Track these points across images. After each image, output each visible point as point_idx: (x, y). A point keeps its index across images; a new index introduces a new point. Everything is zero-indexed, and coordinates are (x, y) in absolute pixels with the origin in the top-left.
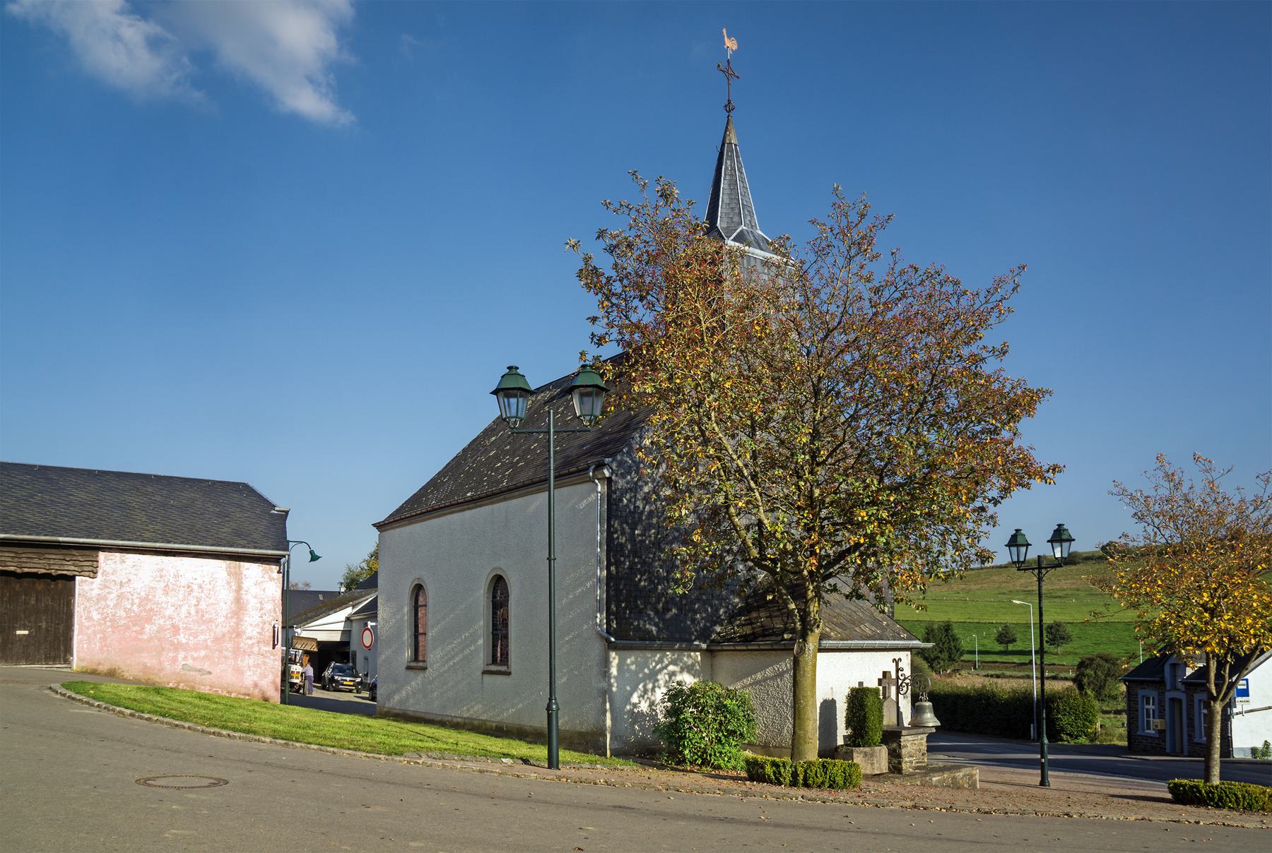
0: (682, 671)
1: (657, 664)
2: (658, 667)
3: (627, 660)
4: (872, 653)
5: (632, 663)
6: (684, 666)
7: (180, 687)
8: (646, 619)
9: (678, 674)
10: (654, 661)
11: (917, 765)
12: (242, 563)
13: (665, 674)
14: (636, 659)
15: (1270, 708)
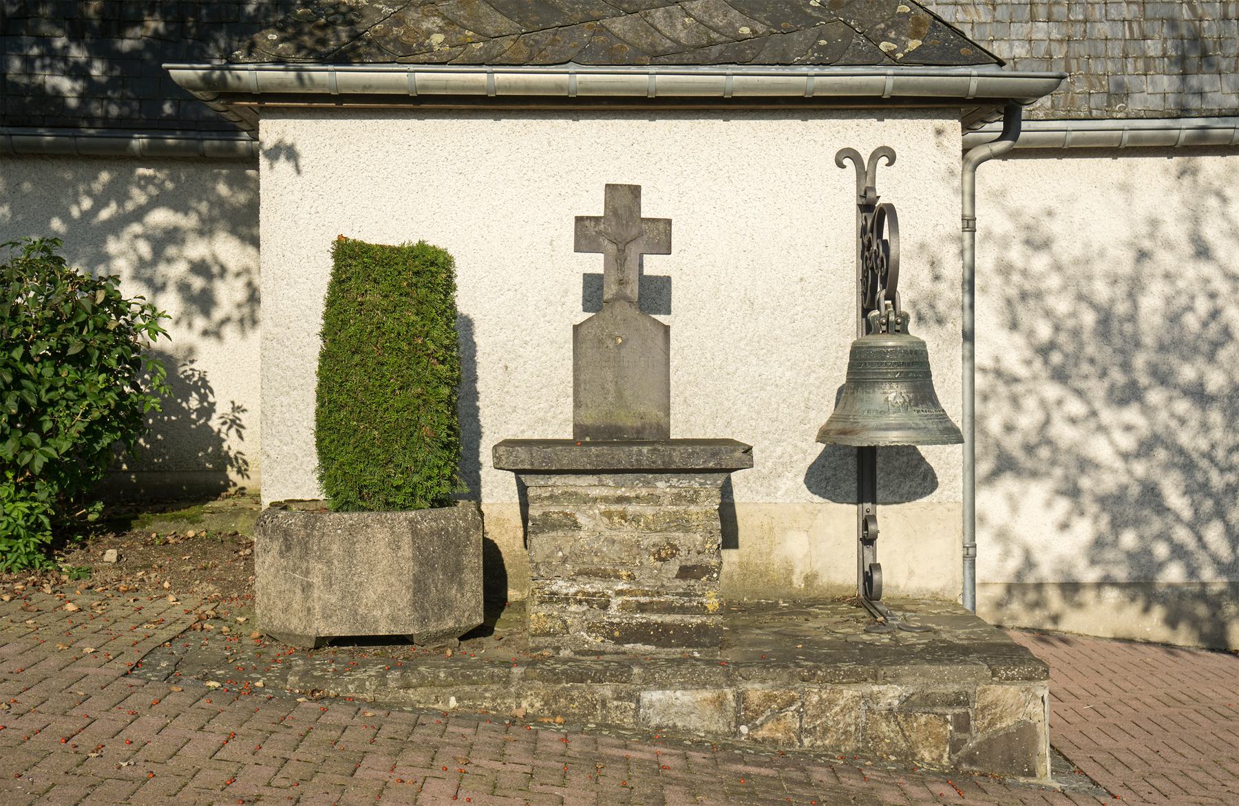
0: (206, 230)
1: (100, 204)
2: (105, 214)
4: (507, 124)
6: (216, 212)
7: (79, 274)
8: (35, 51)
9: (191, 237)
10: (89, 193)
11: (639, 618)
13: (136, 237)
15: (3, 246)
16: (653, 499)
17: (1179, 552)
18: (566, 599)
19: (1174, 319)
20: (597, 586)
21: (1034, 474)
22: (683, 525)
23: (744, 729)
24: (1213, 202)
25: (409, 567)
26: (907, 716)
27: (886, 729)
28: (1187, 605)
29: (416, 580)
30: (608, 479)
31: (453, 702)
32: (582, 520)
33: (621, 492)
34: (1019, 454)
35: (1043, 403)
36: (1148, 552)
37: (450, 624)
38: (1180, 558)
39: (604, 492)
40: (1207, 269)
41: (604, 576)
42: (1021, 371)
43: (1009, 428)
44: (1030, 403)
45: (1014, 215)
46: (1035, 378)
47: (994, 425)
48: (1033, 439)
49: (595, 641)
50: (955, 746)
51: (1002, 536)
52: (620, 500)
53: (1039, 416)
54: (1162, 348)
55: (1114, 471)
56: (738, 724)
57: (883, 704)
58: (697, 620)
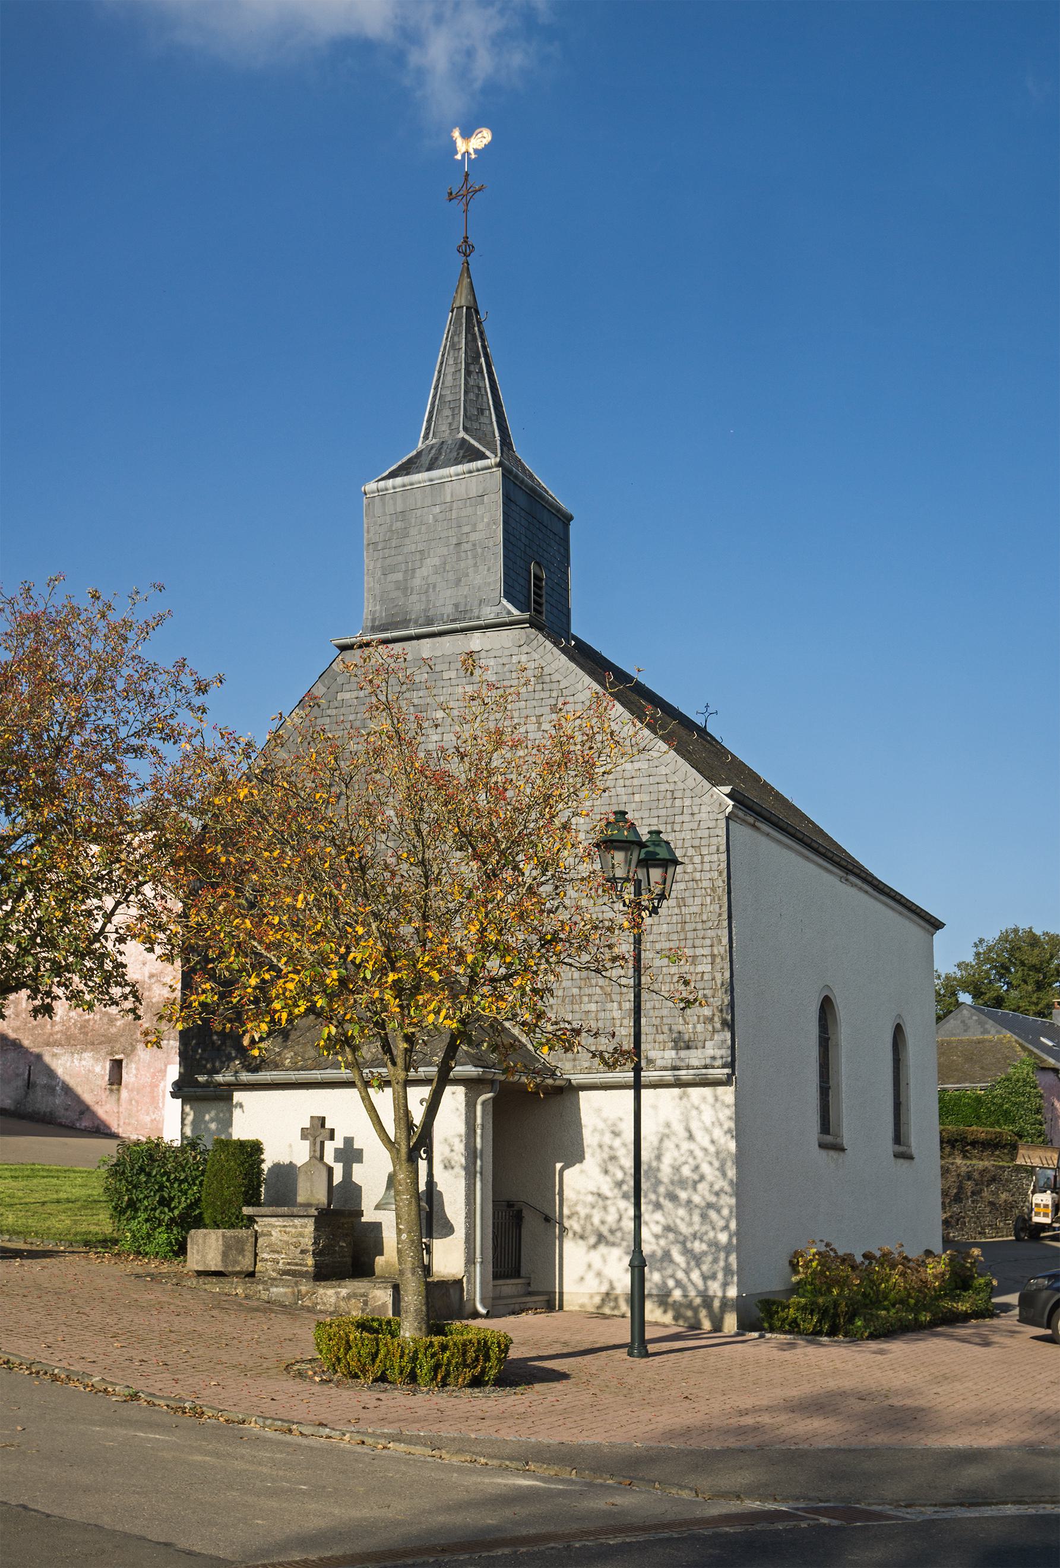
3: (204, 1116)
4: (311, 1091)
5: (212, 1120)
11: (288, 1267)
12: (585, 1144)
14: (217, 1115)
16: (295, 1227)
17: (679, 1284)
18: (266, 1260)
19: (677, 1169)
20: (276, 1256)
21: (613, 1244)
22: (301, 1235)
23: (300, 1302)
24: (694, 1113)
25: (221, 1248)
26: (349, 1300)
27: (342, 1303)
28: (682, 1310)
29: (223, 1252)
30: (280, 1219)
31: (218, 1290)
32: (273, 1233)
33: (285, 1223)
34: (606, 1233)
35: (618, 1210)
36: (665, 1283)
37: (238, 1269)
38: (680, 1287)
39: (280, 1223)
40: (692, 1146)
41: (278, 1252)
42: (609, 1194)
43: (603, 1222)
44: (612, 1210)
45: (605, 1121)
46: (615, 1198)
47: (596, 1220)
48: (614, 1227)
49: (274, 1274)
50: (363, 1311)
51: (599, 1274)
52: (285, 1226)
53: (616, 1216)
54: (672, 1182)
55: (650, 1243)
56: (298, 1300)
57: (342, 1294)
58: (305, 1269)
